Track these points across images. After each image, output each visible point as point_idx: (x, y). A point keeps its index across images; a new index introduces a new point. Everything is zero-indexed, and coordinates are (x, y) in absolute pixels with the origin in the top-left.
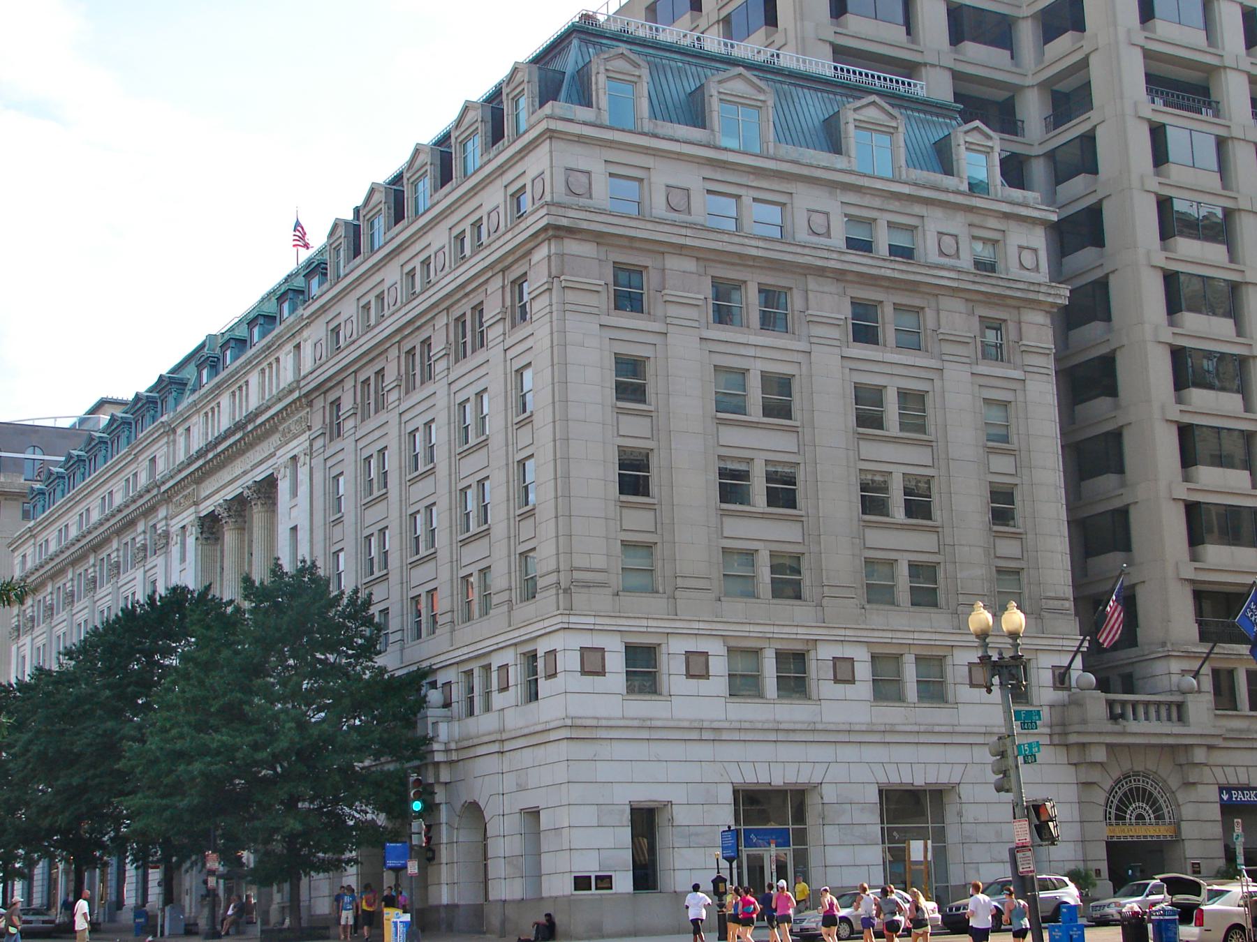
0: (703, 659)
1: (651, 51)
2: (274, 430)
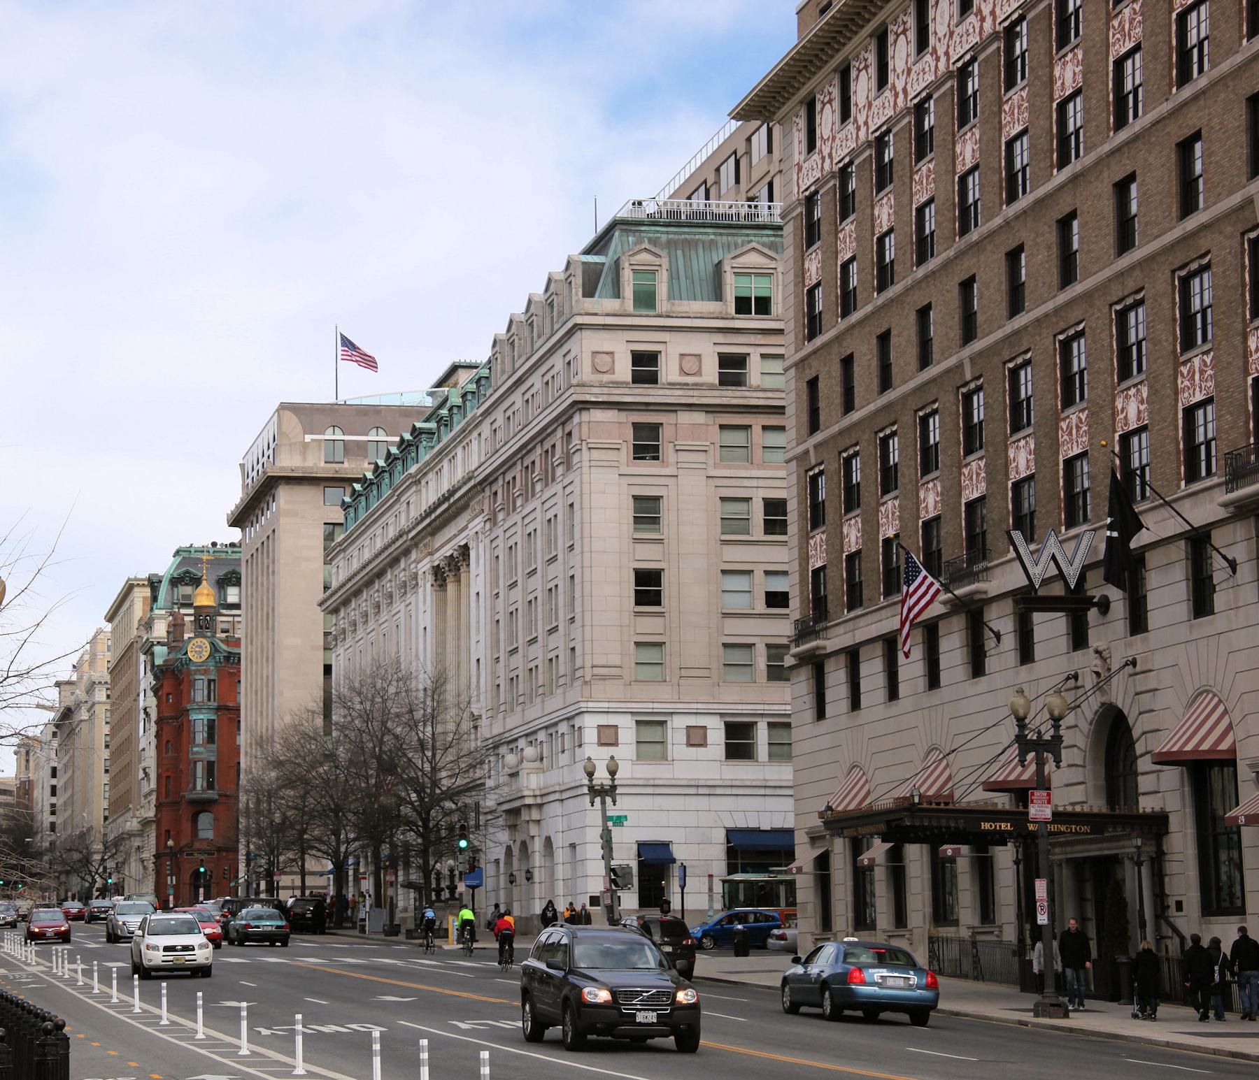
0: (701, 732)
1: (686, 230)
2: (465, 507)
